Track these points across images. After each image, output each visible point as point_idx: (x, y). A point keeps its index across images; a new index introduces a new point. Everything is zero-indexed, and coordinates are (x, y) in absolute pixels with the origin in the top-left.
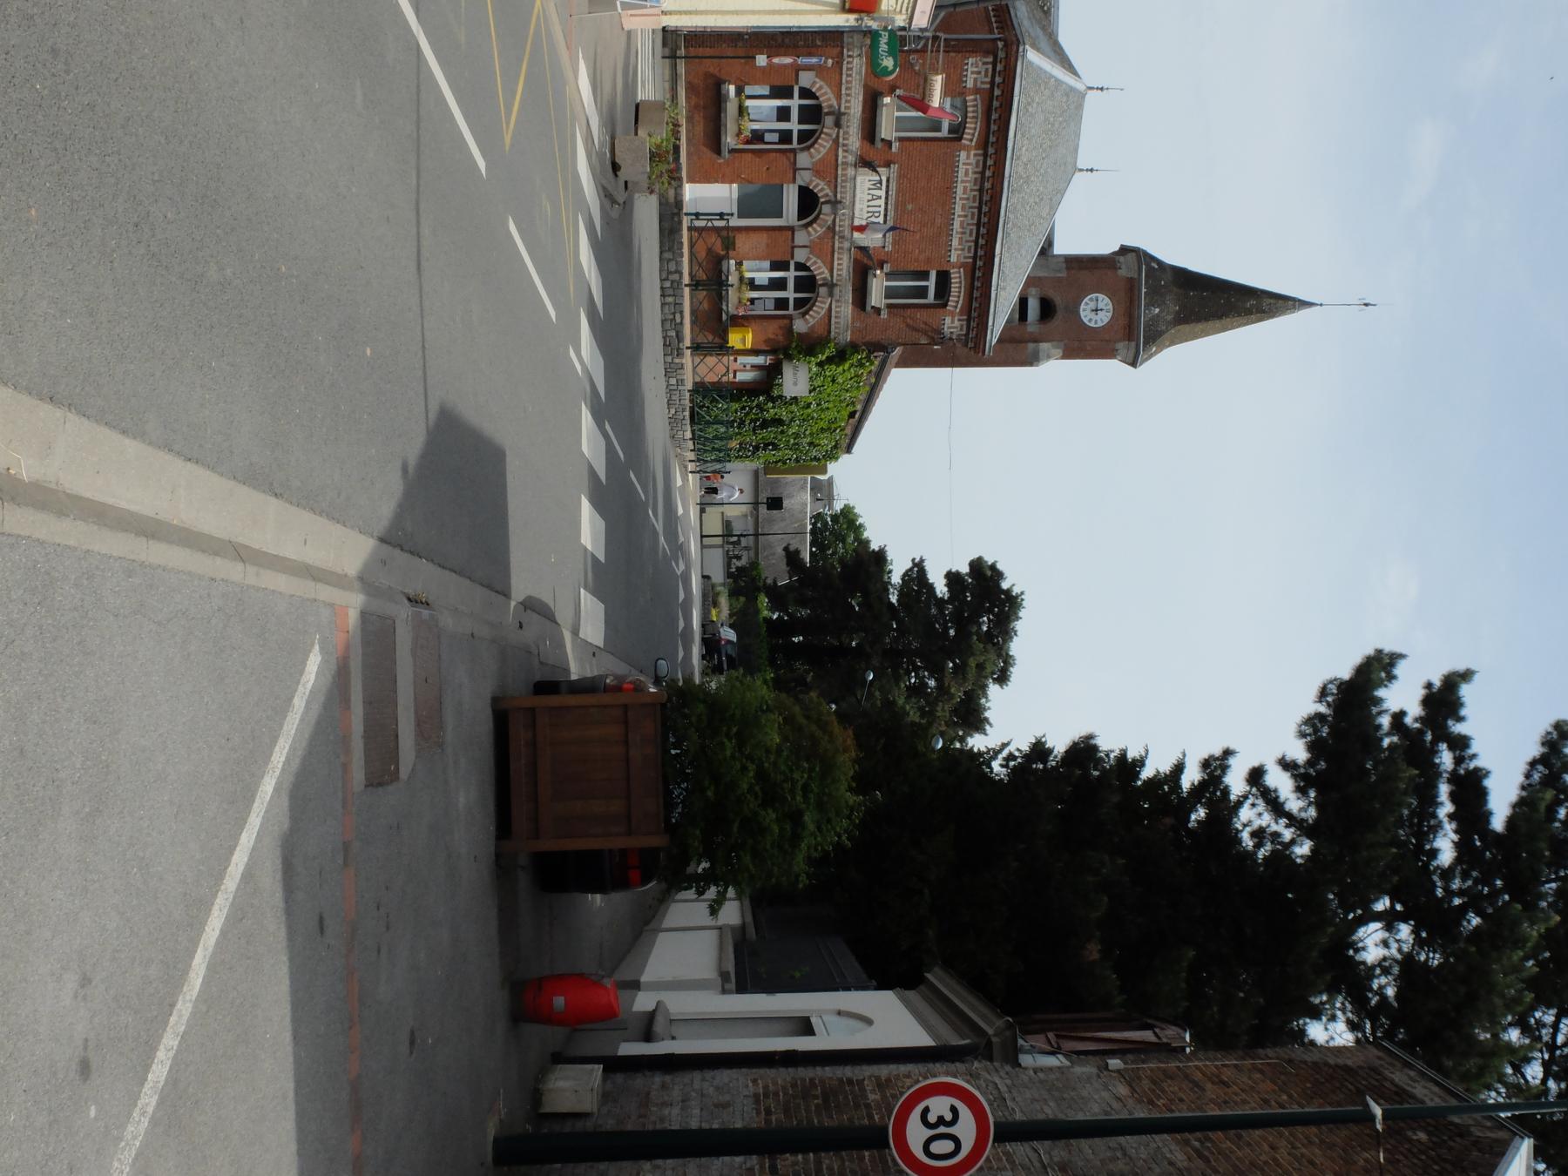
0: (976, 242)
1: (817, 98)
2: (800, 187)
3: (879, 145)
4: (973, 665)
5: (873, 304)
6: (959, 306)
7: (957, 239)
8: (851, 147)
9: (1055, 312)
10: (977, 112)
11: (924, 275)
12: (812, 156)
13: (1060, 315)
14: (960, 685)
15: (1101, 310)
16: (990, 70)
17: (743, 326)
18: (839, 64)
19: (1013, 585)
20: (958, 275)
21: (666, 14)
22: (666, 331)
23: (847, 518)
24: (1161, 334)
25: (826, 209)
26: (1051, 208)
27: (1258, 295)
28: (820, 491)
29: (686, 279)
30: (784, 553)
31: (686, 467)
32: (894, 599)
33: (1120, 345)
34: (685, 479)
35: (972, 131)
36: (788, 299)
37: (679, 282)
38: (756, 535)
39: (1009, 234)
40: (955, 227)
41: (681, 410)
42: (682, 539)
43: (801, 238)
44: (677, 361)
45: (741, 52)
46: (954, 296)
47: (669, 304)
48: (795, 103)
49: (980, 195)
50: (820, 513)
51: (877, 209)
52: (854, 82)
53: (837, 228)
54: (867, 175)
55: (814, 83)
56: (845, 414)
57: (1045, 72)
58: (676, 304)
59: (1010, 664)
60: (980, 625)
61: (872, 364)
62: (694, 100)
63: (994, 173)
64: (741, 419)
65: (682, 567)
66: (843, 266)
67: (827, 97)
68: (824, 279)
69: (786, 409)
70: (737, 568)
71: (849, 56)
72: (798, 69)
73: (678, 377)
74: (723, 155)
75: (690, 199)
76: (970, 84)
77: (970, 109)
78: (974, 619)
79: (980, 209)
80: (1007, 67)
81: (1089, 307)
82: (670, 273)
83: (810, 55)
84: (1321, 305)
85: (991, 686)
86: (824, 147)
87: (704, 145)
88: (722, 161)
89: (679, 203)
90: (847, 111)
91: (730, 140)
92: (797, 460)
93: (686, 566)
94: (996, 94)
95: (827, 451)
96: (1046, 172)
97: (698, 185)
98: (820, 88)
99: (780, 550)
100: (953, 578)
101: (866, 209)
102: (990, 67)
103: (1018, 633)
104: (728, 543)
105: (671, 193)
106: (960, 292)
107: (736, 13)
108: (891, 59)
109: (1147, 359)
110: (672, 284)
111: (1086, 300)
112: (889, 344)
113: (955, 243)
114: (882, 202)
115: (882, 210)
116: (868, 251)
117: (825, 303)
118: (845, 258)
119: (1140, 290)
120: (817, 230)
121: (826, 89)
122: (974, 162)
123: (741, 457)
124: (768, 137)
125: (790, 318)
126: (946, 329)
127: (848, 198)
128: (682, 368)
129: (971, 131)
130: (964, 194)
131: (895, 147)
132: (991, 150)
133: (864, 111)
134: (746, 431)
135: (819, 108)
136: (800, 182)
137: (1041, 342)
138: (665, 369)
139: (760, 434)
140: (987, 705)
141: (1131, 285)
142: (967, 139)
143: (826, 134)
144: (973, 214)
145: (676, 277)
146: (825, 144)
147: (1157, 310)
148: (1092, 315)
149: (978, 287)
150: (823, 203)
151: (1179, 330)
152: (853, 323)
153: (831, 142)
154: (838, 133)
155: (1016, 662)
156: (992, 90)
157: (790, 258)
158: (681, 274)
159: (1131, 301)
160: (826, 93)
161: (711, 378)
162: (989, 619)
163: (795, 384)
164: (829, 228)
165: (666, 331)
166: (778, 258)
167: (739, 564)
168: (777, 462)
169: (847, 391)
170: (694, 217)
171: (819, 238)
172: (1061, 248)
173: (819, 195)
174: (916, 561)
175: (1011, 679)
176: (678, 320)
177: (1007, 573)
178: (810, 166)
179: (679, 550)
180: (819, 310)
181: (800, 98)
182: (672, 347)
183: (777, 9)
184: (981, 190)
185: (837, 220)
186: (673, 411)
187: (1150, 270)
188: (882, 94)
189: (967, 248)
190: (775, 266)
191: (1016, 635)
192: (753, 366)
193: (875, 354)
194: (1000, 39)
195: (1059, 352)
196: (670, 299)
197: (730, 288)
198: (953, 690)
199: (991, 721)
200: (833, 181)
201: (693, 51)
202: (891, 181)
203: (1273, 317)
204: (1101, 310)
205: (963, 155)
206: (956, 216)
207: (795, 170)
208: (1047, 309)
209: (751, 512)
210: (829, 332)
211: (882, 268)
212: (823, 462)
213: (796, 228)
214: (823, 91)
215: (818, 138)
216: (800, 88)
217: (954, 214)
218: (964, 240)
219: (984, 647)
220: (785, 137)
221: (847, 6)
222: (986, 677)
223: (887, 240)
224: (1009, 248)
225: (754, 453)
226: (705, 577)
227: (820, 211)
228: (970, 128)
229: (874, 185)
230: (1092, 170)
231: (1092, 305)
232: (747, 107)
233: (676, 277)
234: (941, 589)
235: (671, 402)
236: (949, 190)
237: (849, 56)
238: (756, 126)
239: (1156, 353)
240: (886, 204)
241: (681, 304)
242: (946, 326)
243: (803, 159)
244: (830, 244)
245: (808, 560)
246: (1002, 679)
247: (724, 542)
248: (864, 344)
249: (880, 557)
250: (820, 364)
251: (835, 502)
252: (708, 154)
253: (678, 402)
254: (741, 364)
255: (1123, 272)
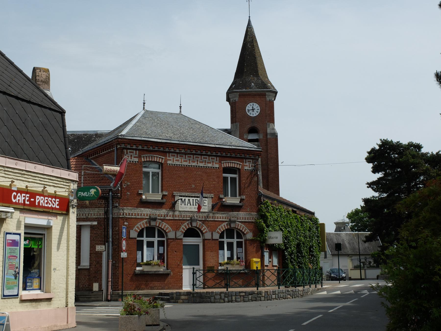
0: (209, 156)
1: (224, 231)
2: (184, 236)
3: (164, 200)
4: (413, 160)
5: (239, 202)
6: (239, 163)
7: (208, 164)
8: (166, 213)
9: (254, 127)
10: (149, 156)
11: (225, 179)
12: (170, 231)
13: (256, 125)
14: (422, 165)
15: (253, 107)
16: (130, 151)
17: (250, 262)
18: (127, 219)
19: (377, 144)
20: (225, 164)
21: (68, 305)
22: (249, 300)
23: (354, 216)
24: (262, 82)
25: (194, 224)
26: (196, 124)
27: (246, 43)
28: (340, 228)
29: (224, 290)
30: (367, 243)
31: (318, 289)
32: (385, 195)
33: (268, 99)
34: (323, 290)
35: (158, 158)
36: (237, 242)
37: (225, 293)
38: (360, 255)
39: (206, 141)
40: (203, 165)
41: (288, 292)
42: (352, 292)
43: (208, 236)
44: (263, 295)
45: (120, 265)
46: (235, 165)
47: (236, 299)
48: (145, 239)
49: (187, 154)
50: (351, 228)
51: (194, 201)
52: (135, 212)
53: (203, 219)
54: (178, 205)
55: (136, 230)
56: (293, 215)
57: (133, 127)
58: (236, 295)
59: (412, 144)
60: (395, 158)
61: (267, 202)
62: (143, 286)
63: (177, 148)
64: (297, 263)
65: (366, 292)
66: (221, 216)
67: (142, 225)
68: (227, 225)
69: (291, 242)
70: (374, 263)
71: (123, 215)
72: (129, 238)
73: (271, 294)
74: (169, 273)
75: (190, 288)
76: (137, 160)
77: (148, 160)
78: (393, 161)
79: (193, 154)
80: (129, 143)
81: (252, 113)
82: (221, 298)
83: (122, 232)
84: (249, 17)
85: (422, 152)
86: (165, 225)
87: (164, 282)
88: (172, 273)
89: (188, 293)
90: (149, 215)
91: (162, 269)
92: (318, 237)
93: (366, 289)
94: (141, 148)
95: (313, 223)
96: (179, 126)
97: (183, 284)
98: (138, 227)
99: (367, 244)
100: (375, 170)
101: (195, 206)
102: (128, 151)
103: (398, 141)
104: (364, 267)
105: (183, 297)
106: (233, 163)
107: (68, 268)
108: (91, 190)
109: (273, 87)
110: (226, 297)
111: (249, 114)
112: (258, 194)
113: (210, 165)
114: (191, 199)
115: (194, 199)
116: (214, 205)
117: (239, 225)
118: (217, 215)
119: (244, 92)
120: (204, 228)
121: (138, 225)
122: (172, 157)
123: (317, 262)
124: (161, 251)
125: (246, 240)
126: (250, 169)
127: (189, 214)
128: (267, 292)
129: (158, 159)
130: (175, 156)
131: (165, 193)
132: (167, 150)
133: (148, 208)
134: (304, 261)
135: (147, 228)
136: (182, 237)
137: (267, 132)
138: (268, 300)
139: (305, 254)
140: (430, 153)
141: (242, 95)
142: (162, 161)
143: (159, 224)
144: (196, 157)
145: (223, 295)
146: (164, 225)
147: (252, 84)
148: (255, 111)
149: (230, 155)
150: (192, 226)
151: (261, 74)
152: (248, 212)
153: (163, 223)
154: (158, 219)
155: (411, 141)
156: (139, 150)
157: (218, 241)
158: (221, 293)
159: (249, 95)
160: (140, 225)
161: (274, 278)
162: (392, 154)
163: (277, 238)
164: (203, 223)
165: (249, 300)
166: (218, 247)
167: (373, 263)
168: (319, 246)
169: (281, 214)
170: (195, 286)
171: (208, 227)
172: (228, 126)
173: (188, 227)
174: (368, 186)
175: (418, 143)
176: (244, 294)
177: (372, 147)
178: (174, 232)
179: (357, 292)
180: (242, 227)
181: (143, 237)
182: (256, 297)
183: (66, 247)
184: (186, 154)
185: (200, 219)
186: (289, 296)
187: (235, 88)
188: (141, 199)
189: (212, 160)
190: (222, 249)
191: (399, 142)
192: (270, 258)
193: (263, 201)
194: (117, 147)
195: (271, 124)
196: (234, 298)
197: (228, 269)
198: (424, 169)
199: (437, 151)
200: (181, 221)
201: (120, 287)
202: (181, 195)
203: (255, 36)
204: (253, 107)
205: (169, 162)
206: (198, 165)
207: (176, 239)
208: (253, 130)
209: (350, 257)
210: (252, 222)
211: (222, 198)
212: (318, 225)
213: (204, 238)
214: (139, 226)
215: (161, 228)
216: (219, 238)
217: (196, 166)
218: (208, 161)
219: (405, 156)
220: (161, 244)
221: (65, 212)
222: (418, 154)
223: (209, 196)
224: (212, 141)
225: (315, 257)
226: (378, 278)
227: (196, 227)
228: (157, 159)
229: (183, 203)
230: (180, 107)
231: (251, 111)
232: (147, 261)
233: (223, 295)
234: (380, 175)
235: (284, 297)
236: (186, 168)
237: (123, 215)
238: (156, 257)
239: (271, 84)
240: (192, 197)
241: (236, 292)
242: (249, 169)
243: (171, 235)
244: (211, 222)
245: (370, 232)
246: (419, 147)
247: (363, 269)
248: (257, 206)
249: (366, 201)
250: (268, 226)
251: (345, 221)
252: (169, 279)
253: (284, 294)
254: (269, 264)
255: (237, 99)
